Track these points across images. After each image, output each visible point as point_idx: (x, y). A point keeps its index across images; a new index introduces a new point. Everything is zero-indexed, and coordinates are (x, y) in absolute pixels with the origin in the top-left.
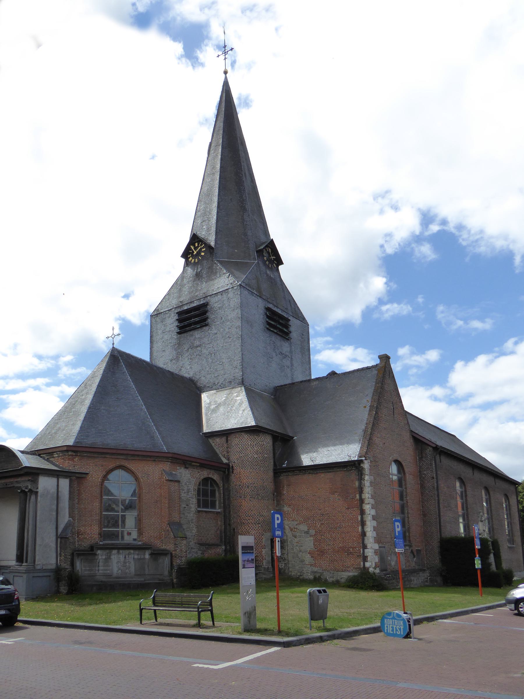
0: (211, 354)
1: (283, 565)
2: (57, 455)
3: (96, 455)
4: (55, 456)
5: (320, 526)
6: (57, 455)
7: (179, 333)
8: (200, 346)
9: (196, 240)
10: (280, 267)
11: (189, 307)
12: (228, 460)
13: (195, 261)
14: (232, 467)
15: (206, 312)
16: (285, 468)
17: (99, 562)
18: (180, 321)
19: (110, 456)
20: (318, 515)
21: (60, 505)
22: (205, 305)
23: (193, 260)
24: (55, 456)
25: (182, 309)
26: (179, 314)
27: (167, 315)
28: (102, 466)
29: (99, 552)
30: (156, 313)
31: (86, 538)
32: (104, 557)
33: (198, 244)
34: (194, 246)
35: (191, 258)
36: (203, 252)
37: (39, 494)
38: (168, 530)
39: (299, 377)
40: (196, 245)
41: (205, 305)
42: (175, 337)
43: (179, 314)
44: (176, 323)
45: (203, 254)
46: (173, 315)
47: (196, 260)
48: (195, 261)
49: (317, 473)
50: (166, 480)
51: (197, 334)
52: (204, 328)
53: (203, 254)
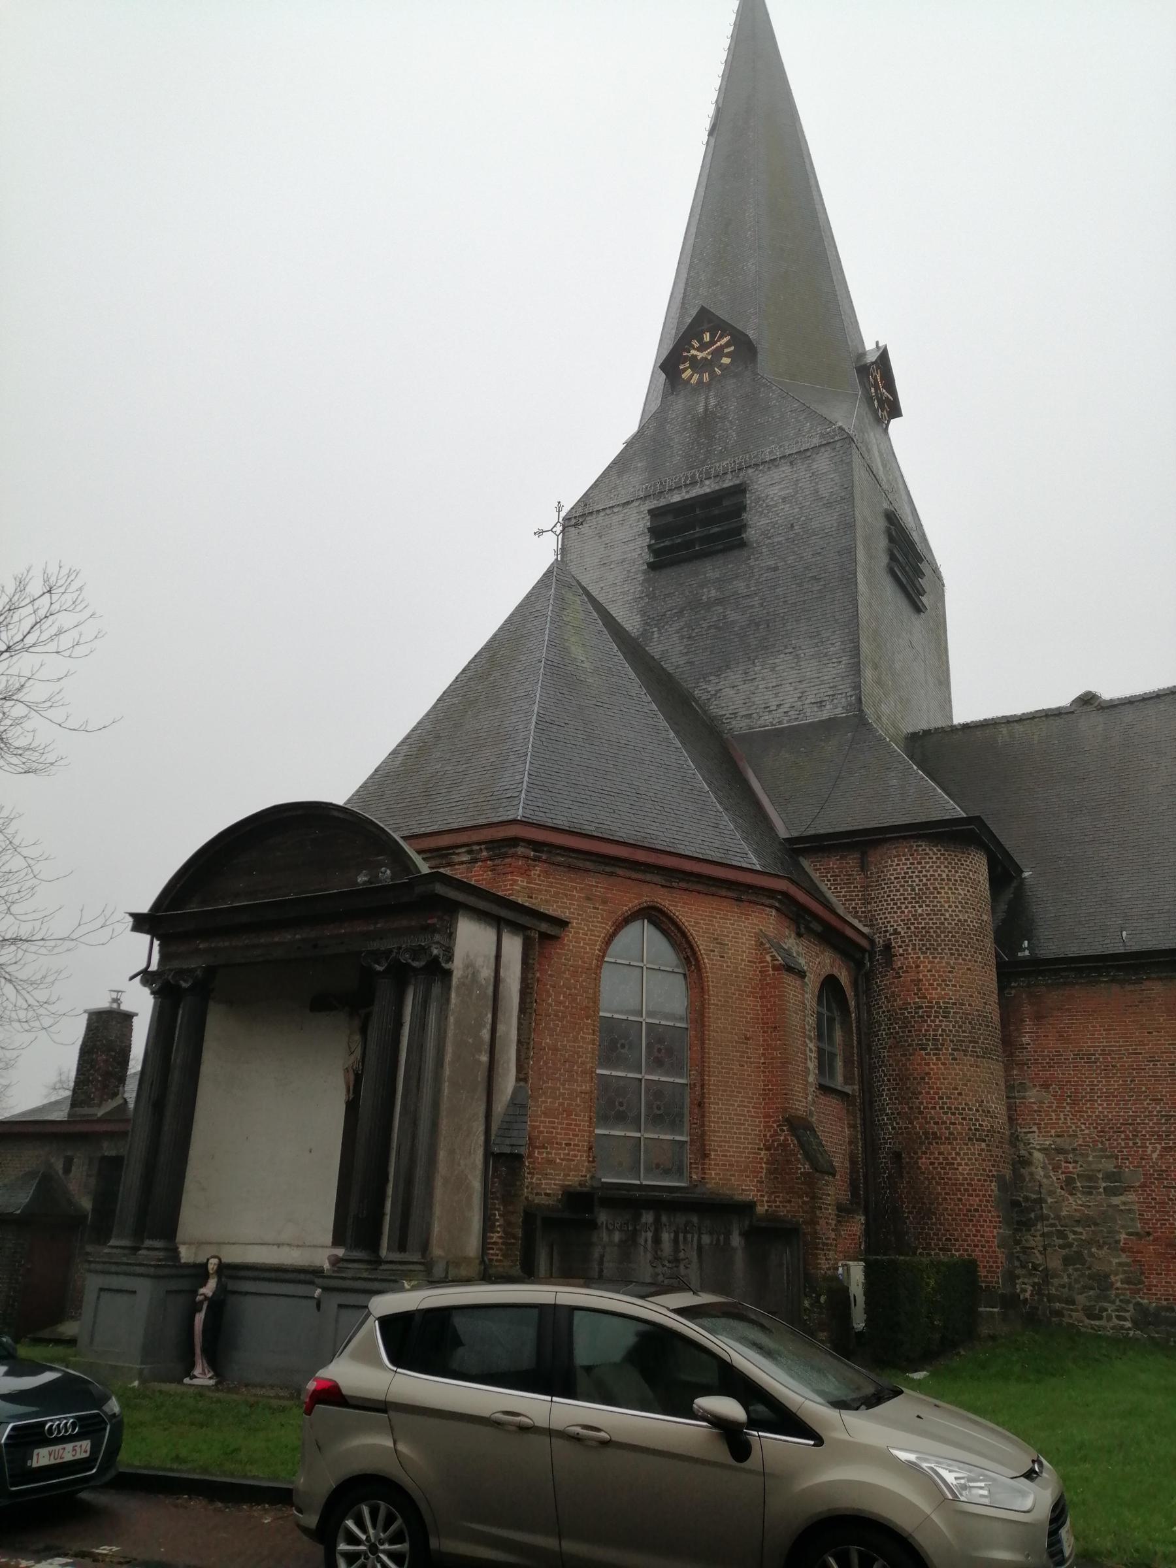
0: (757, 625)
1: (1030, 1288)
2: (466, 858)
3: (589, 865)
4: (456, 859)
5: (1161, 1156)
6: (466, 858)
7: (652, 567)
8: (719, 601)
9: (706, 326)
10: (894, 423)
11: (687, 497)
12: (871, 926)
13: (701, 378)
14: (888, 947)
15: (741, 508)
16: (1025, 962)
17: (601, 1262)
18: (654, 532)
19: (628, 874)
20: (1150, 1116)
21: (501, 1028)
22: (740, 490)
23: (696, 376)
24: (456, 859)
25: (663, 502)
26: (653, 513)
27: (616, 519)
28: (604, 902)
29: (603, 1217)
30: (580, 512)
31: (550, 1162)
32: (617, 1237)
33: (712, 336)
34: (700, 340)
35: (689, 372)
36: (728, 355)
37: (454, 981)
38: (784, 1145)
39: (941, 723)
40: (707, 337)
41: (740, 490)
42: (641, 577)
43: (653, 513)
44: (646, 540)
45: (726, 361)
46: (634, 517)
47: (706, 378)
48: (701, 378)
49: (1139, 981)
50: (775, 968)
51: (711, 570)
52: (736, 553)
53: (726, 361)
